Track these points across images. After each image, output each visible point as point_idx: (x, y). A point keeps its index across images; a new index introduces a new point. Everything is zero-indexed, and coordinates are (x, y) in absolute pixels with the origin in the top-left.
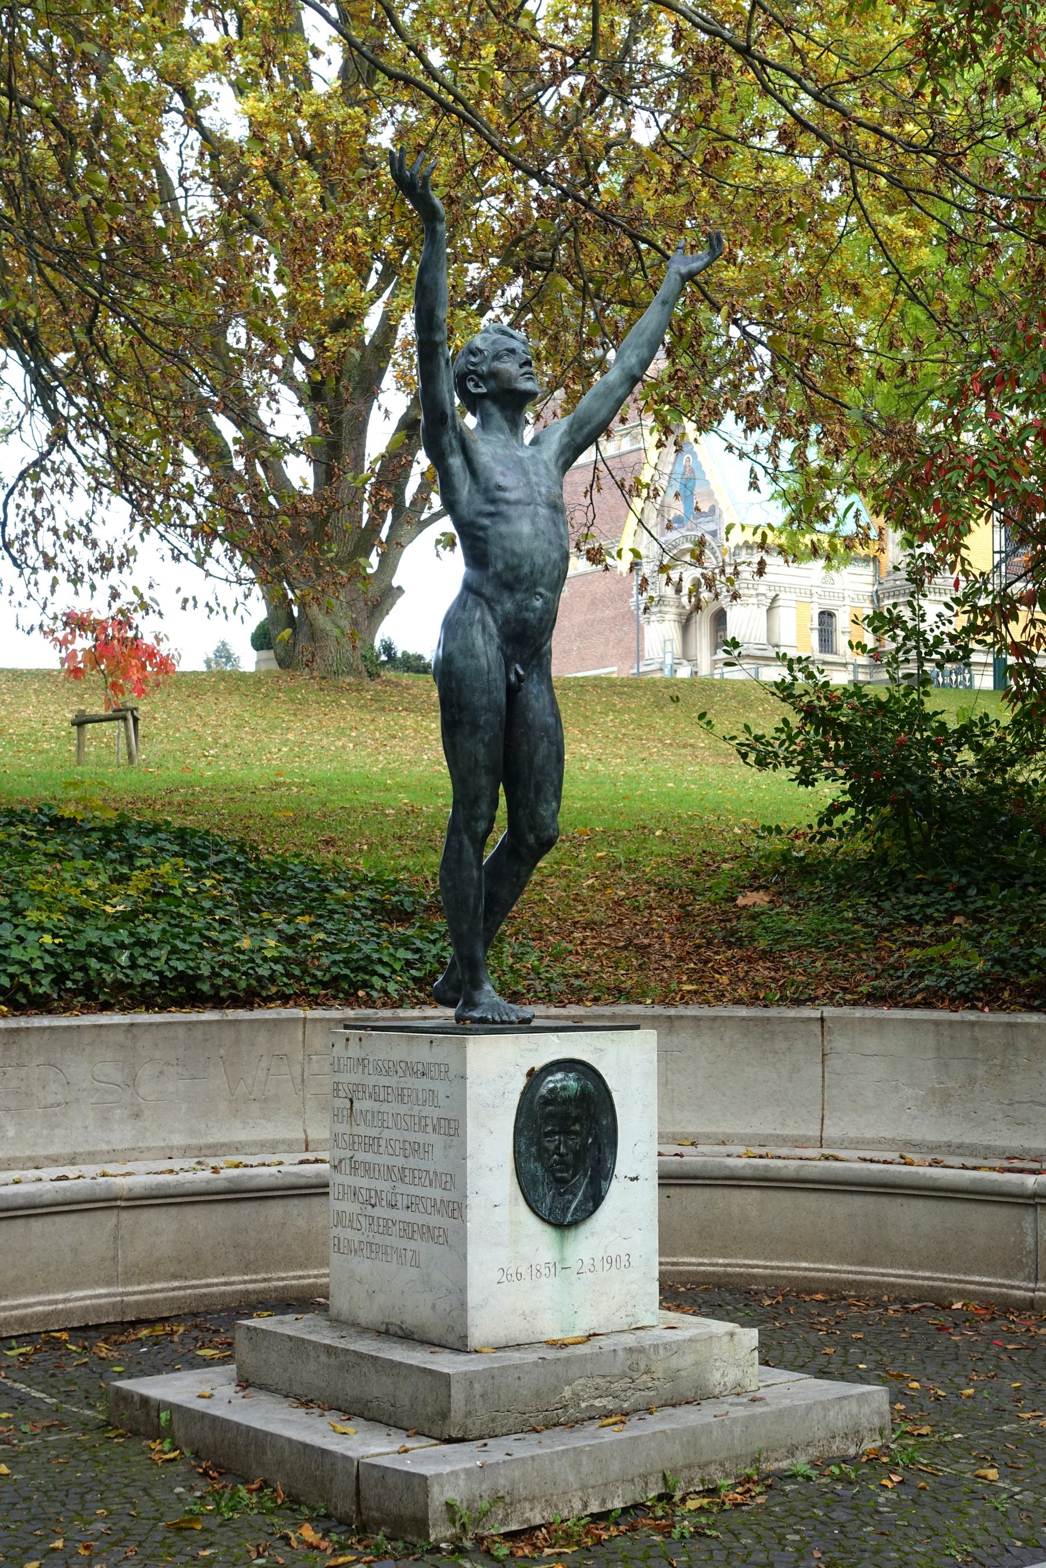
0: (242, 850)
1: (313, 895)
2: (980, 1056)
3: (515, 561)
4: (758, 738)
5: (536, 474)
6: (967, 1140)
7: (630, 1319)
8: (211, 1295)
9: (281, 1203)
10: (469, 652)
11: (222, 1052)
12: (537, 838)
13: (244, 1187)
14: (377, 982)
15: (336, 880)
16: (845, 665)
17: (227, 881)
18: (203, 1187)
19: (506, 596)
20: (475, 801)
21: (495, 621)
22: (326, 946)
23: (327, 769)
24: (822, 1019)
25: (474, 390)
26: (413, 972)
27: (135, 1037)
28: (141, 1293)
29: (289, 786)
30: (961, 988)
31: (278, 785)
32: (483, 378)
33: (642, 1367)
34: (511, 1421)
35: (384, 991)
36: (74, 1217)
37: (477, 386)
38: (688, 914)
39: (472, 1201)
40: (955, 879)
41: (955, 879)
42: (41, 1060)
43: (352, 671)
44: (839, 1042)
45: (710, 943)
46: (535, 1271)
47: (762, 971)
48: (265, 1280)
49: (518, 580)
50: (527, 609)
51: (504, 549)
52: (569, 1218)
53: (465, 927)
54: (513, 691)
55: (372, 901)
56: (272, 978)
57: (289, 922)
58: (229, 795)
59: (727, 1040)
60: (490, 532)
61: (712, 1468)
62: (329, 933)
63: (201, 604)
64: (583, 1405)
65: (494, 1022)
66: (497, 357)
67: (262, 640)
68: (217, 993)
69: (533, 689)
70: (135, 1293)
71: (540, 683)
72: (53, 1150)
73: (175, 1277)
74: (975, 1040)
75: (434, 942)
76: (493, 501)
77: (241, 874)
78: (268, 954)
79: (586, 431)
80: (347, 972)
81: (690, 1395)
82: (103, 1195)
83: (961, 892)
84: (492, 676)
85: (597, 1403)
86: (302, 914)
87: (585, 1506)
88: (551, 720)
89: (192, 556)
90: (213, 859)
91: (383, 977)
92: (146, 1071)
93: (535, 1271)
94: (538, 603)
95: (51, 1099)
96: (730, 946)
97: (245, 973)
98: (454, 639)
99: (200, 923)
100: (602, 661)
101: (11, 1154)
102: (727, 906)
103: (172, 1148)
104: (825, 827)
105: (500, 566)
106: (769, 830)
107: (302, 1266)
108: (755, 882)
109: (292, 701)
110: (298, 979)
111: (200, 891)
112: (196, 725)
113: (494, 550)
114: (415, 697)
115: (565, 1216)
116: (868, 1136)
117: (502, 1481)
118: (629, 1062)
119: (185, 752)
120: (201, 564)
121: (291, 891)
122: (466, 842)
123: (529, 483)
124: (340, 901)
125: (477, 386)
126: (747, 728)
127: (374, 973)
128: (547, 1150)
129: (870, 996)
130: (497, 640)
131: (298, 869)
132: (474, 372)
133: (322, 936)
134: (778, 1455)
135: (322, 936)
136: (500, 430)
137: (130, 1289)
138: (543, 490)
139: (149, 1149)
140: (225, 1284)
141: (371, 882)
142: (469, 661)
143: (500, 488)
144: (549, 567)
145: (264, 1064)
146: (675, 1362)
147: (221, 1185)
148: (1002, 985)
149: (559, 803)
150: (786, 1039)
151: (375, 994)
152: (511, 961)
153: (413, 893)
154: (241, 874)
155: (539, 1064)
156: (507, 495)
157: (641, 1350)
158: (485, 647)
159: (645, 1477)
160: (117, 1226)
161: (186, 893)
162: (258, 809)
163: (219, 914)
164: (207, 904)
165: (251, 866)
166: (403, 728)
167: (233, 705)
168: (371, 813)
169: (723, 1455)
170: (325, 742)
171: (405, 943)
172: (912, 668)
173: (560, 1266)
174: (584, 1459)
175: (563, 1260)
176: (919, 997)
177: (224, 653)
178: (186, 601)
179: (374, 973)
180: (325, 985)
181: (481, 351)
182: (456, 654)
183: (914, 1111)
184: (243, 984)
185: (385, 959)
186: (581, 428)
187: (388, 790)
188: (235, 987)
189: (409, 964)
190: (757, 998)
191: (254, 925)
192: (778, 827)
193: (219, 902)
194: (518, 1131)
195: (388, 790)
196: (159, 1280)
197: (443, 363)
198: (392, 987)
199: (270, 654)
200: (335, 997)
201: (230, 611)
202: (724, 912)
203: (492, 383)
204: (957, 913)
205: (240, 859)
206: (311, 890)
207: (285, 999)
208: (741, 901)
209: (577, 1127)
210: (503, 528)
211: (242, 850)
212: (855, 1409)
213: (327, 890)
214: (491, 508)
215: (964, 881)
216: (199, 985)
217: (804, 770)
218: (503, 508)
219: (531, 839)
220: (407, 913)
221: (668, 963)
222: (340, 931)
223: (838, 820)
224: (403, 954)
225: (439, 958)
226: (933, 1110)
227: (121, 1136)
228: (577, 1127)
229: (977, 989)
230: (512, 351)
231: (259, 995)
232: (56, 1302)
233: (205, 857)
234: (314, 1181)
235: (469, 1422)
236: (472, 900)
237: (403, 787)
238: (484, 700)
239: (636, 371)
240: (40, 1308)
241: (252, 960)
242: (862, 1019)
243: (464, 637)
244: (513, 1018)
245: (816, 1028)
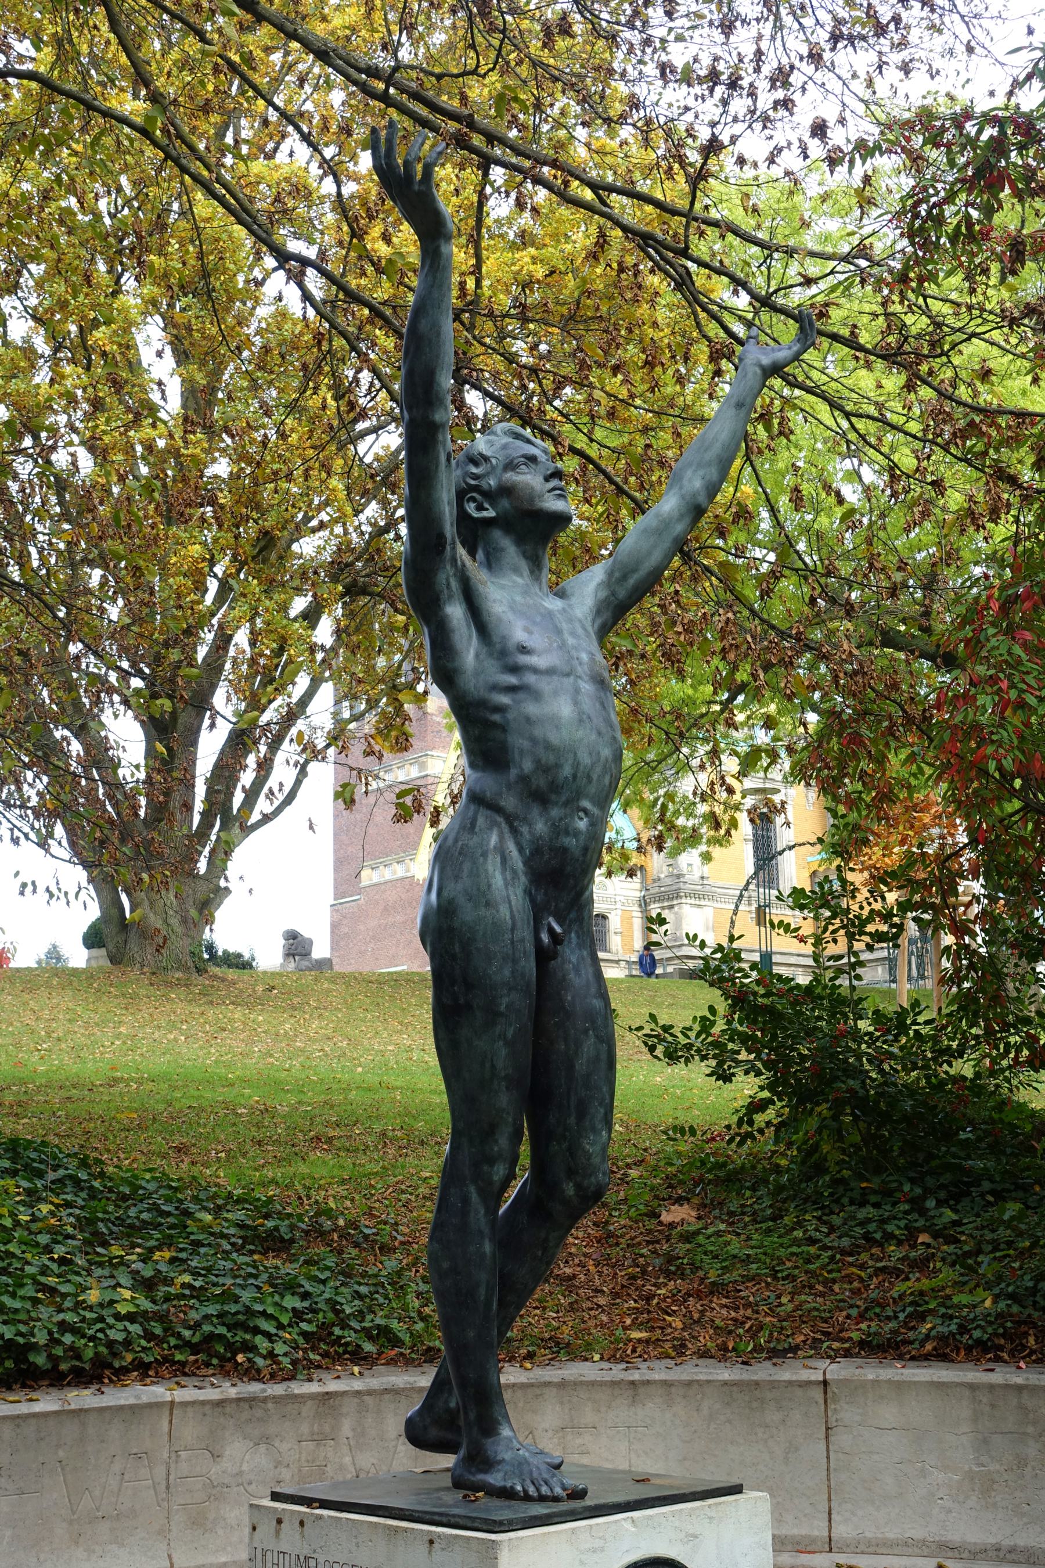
0: (84, 1164)
1: (171, 1220)
2: (1030, 1429)
3: (552, 759)
4: (667, 1029)
5: (573, 634)
6: (1021, 1541)
10: (482, 897)
12: (578, 1187)
14: (260, 1341)
15: (196, 1199)
16: (617, 962)
17: (68, 1205)
19: (535, 811)
20: (490, 1132)
21: (521, 850)
22: (198, 1293)
23: (160, 1063)
24: (825, 1383)
25: (476, 515)
26: (304, 1326)
29: (127, 1082)
30: (977, 1334)
31: (116, 1081)
32: (490, 496)
35: (271, 1355)
37: (480, 508)
38: (610, 1235)
40: (907, 1188)
41: (907, 1188)
43: (182, 966)
44: (846, 1413)
45: (644, 1272)
47: (720, 1312)
49: (555, 787)
50: (567, 833)
51: (534, 741)
53: (471, 1334)
54: (545, 956)
55: (241, 1226)
56: (127, 1343)
57: (145, 1259)
58: (63, 1093)
59: (705, 1411)
60: (510, 716)
62: (195, 1274)
63: (41, 889)
65: (527, 1498)
66: (511, 466)
67: (93, 939)
68: (55, 1367)
69: (571, 954)
71: (580, 946)
74: (1021, 1407)
75: (323, 1282)
76: (515, 669)
77: (84, 1195)
78: (123, 1309)
79: (631, 582)
80: (222, 1330)
83: (917, 1205)
84: (518, 935)
86: (159, 1248)
88: (597, 1003)
89: (32, 836)
90: (51, 1176)
91: (268, 1335)
94: (582, 824)
96: (669, 1275)
97: (92, 1338)
98: (457, 878)
99: (35, 1263)
100: (393, 960)
102: (651, 1224)
104: (746, 1128)
105: (528, 765)
106: (682, 1131)
108: (674, 1190)
109: (123, 995)
110: (159, 1341)
111: (34, 1219)
112: (29, 1019)
113: (518, 742)
114: (241, 991)
116: (891, 1535)
119: (18, 1046)
120: (43, 844)
121: (145, 1216)
122: (474, 1197)
123: (563, 646)
124: (205, 1228)
125: (480, 508)
126: (653, 1017)
127: (256, 1331)
129: (862, 1344)
130: (523, 879)
131: (151, 1187)
132: (476, 489)
133: (187, 1278)
135: (187, 1278)
136: (516, 570)
138: (584, 657)
141: (239, 1201)
142: (483, 911)
143: (523, 650)
144: (598, 770)
145: (117, 1467)
148: (1024, 1328)
149: (610, 1129)
150: (780, 1408)
151: (260, 1362)
152: (417, 1303)
153: (289, 1215)
154: (84, 1195)
156: (533, 660)
158: (504, 887)
161: (17, 1223)
162: (98, 1110)
163: (59, 1251)
164: (43, 1239)
165: (96, 1184)
166: (232, 1021)
167: (65, 1000)
168: (221, 1113)
170: (157, 1035)
171: (291, 1287)
172: (841, 947)
176: (929, 1347)
177: (54, 953)
178: (24, 885)
179: (256, 1331)
180: (195, 1349)
181: (486, 459)
182: (461, 900)
183: (948, 1503)
184: (89, 1353)
185: (270, 1310)
186: (624, 577)
187: (232, 1085)
188: (78, 1357)
189: (298, 1315)
190: (726, 1350)
191: (100, 1264)
192: (691, 1128)
193: (58, 1235)
195: (232, 1085)
197: (443, 458)
198: (280, 1348)
199: (103, 952)
200: (208, 1365)
201: (71, 897)
202: (650, 1232)
203: (505, 503)
204: (920, 1231)
205: (83, 1175)
206: (169, 1214)
207: (144, 1370)
208: (665, 1217)
210: (531, 709)
211: (84, 1164)
213: (187, 1213)
214: (512, 680)
215: (918, 1191)
216: (32, 1358)
217: (720, 1064)
218: (531, 679)
219: (569, 1189)
220: (282, 1240)
221: (602, 1301)
222: (209, 1270)
223: (760, 1119)
224: (291, 1302)
225: (332, 1303)
226: (973, 1501)
229: (996, 1334)
230: (532, 459)
231: (110, 1366)
233: (41, 1174)
236: (482, 1291)
237: (246, 1081)
238: (507, 972)
239: (702, 499)
241: (101, 1319)
242: (876, 1382)
243: (475, 874)
244: (558, 1491)
245: (818, 1394)
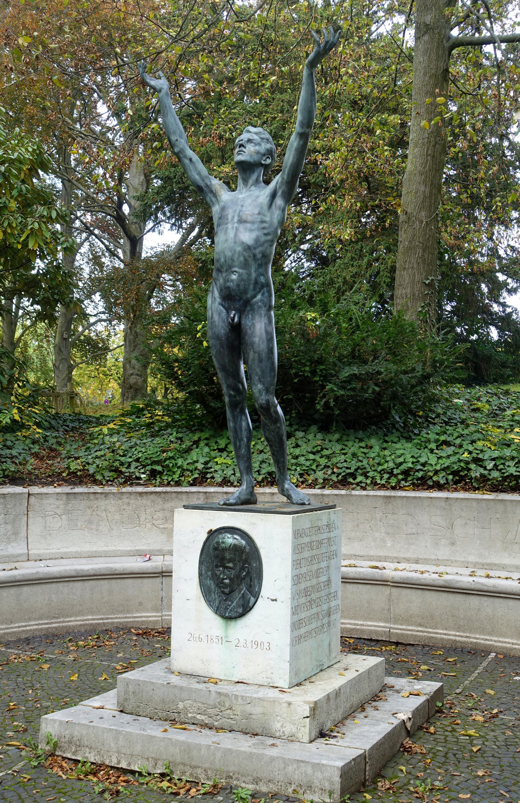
7: (269, 680)
8: (436, 638)
9: (478, 598)
11: (498, 516)
13: (453, 586)
18: (430, 582)
27: (450, 504)
28: (401, 629)
33: (227, 705)
34: (148, 711)
36: (368, 587)
39: (175, 594)
42: (404, 512)
46: (210, 639)
48: (467, 637)
61: (199, 771)
64: (190, 715)
70: (397, 629)
72: (408, 555)
73: (420, 625)
81: (259, 731)
82: (379, 578)
85: (198, 717)
87: (119, 763)
92: (458, 522)
93: (210, 639)
95: (410, 531)
101: (387, 554)
103: (468, 562)
107: (489, 634)
117: (76, 733)
118: (272, 534)
134: (247, 780)
137: (396, 626)
139: (456, 561)
140: (445, 634)
144: (236, 256)
146: (248, 708)
147: (441, 583)
157: (226, 695)
159: (156, 761)
160: (390, 594)
169: (207, 765)
173: (224, 640)
174: (121, 738)
175: (227, 636)
194: (201, 562)
196: (412, 625)
209: (231, 565)
212: (309, 771)
227: (444, 553)
228: (231, 565)
232: (357, 625)
234: (492, 589)
235: (126, 704)
240: (349, 626)
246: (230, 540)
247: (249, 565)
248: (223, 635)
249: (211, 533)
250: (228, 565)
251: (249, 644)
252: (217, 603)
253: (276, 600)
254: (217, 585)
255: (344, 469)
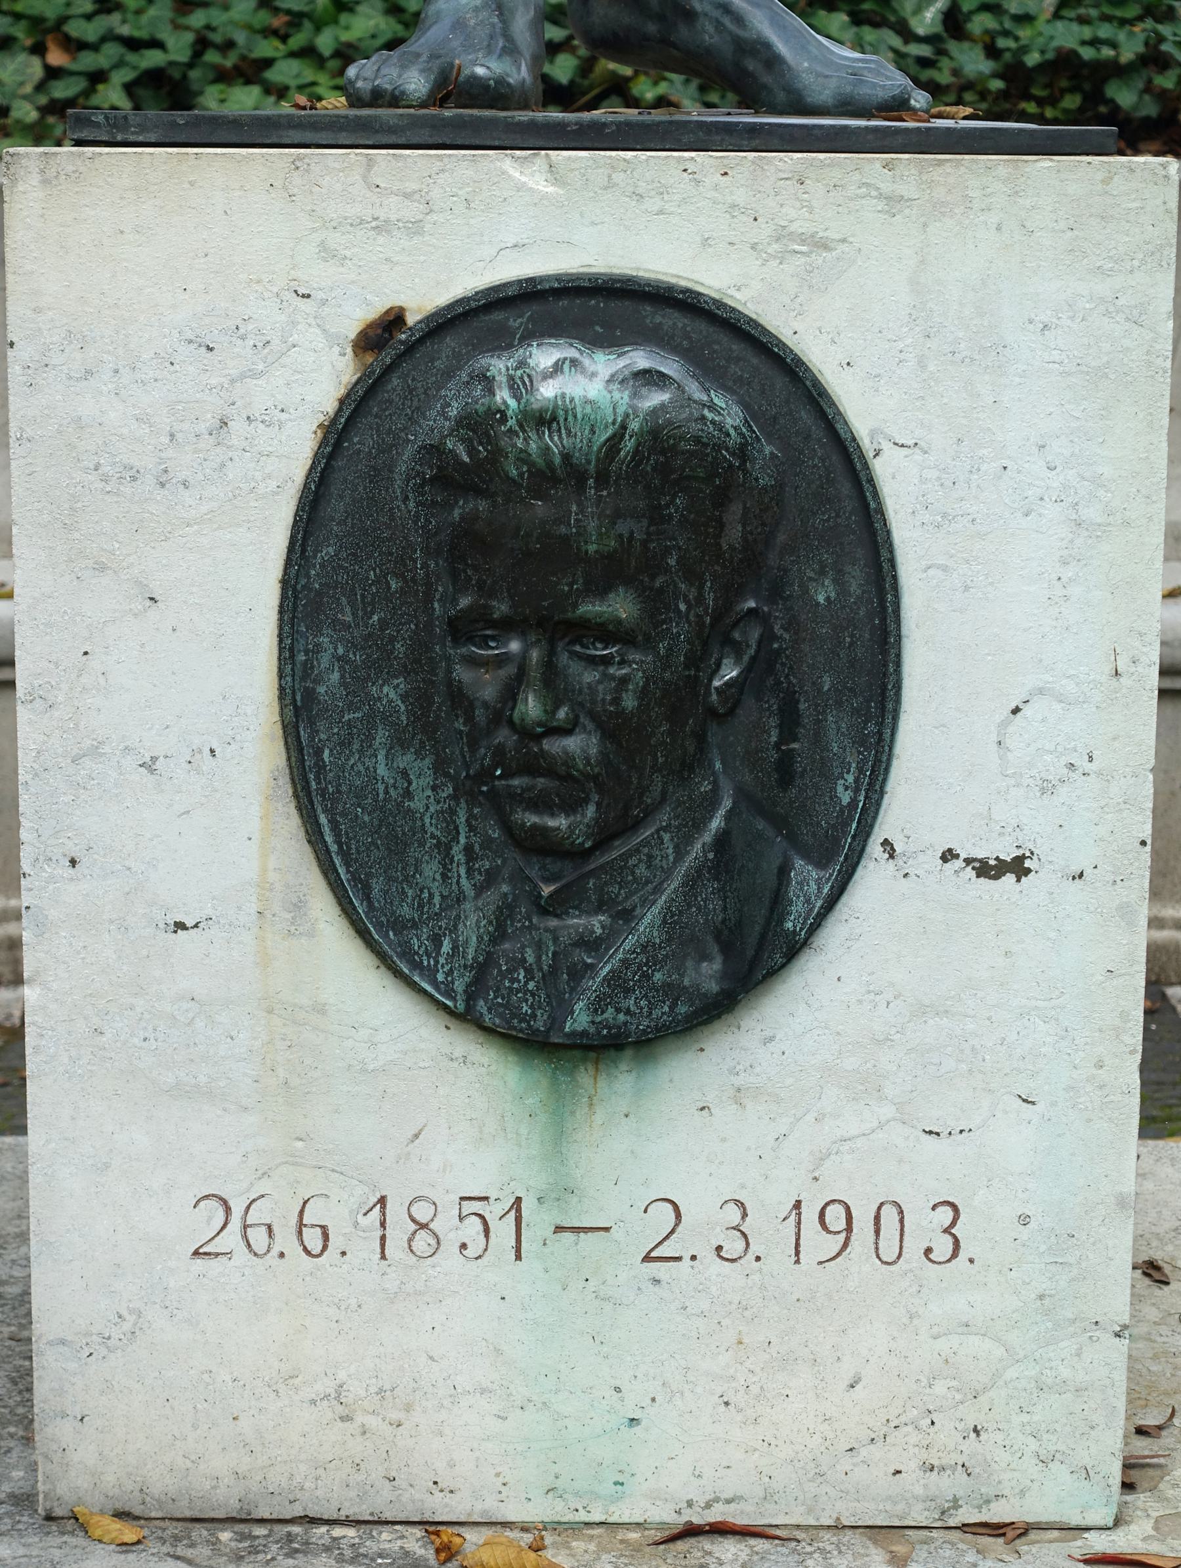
7: (947, 1485)
52: (580, 1019)
115: (560, 1008)
128: (459, 698)
155: (425, 294)
173: (533, 1222)
175: (563, 1191)
194: (303, 603)
209: (620, 606)
228: (620, 606)
246: (584, 383)
247: (776, 593)
248: (529, 1181)
249: (384, 336)
250: (590, 608)
251: (770, 1235)
252: (472, 927)
253: (1018, 867)
254: (475, 788)
255: (112, 51)
